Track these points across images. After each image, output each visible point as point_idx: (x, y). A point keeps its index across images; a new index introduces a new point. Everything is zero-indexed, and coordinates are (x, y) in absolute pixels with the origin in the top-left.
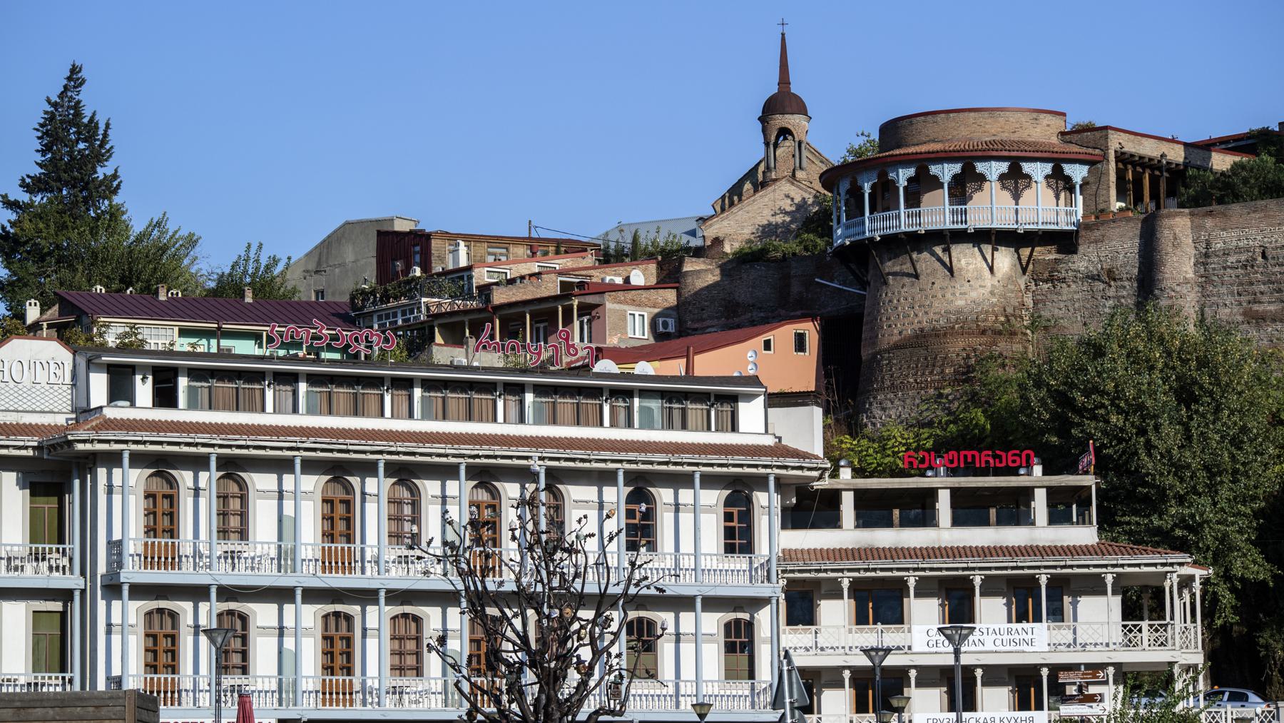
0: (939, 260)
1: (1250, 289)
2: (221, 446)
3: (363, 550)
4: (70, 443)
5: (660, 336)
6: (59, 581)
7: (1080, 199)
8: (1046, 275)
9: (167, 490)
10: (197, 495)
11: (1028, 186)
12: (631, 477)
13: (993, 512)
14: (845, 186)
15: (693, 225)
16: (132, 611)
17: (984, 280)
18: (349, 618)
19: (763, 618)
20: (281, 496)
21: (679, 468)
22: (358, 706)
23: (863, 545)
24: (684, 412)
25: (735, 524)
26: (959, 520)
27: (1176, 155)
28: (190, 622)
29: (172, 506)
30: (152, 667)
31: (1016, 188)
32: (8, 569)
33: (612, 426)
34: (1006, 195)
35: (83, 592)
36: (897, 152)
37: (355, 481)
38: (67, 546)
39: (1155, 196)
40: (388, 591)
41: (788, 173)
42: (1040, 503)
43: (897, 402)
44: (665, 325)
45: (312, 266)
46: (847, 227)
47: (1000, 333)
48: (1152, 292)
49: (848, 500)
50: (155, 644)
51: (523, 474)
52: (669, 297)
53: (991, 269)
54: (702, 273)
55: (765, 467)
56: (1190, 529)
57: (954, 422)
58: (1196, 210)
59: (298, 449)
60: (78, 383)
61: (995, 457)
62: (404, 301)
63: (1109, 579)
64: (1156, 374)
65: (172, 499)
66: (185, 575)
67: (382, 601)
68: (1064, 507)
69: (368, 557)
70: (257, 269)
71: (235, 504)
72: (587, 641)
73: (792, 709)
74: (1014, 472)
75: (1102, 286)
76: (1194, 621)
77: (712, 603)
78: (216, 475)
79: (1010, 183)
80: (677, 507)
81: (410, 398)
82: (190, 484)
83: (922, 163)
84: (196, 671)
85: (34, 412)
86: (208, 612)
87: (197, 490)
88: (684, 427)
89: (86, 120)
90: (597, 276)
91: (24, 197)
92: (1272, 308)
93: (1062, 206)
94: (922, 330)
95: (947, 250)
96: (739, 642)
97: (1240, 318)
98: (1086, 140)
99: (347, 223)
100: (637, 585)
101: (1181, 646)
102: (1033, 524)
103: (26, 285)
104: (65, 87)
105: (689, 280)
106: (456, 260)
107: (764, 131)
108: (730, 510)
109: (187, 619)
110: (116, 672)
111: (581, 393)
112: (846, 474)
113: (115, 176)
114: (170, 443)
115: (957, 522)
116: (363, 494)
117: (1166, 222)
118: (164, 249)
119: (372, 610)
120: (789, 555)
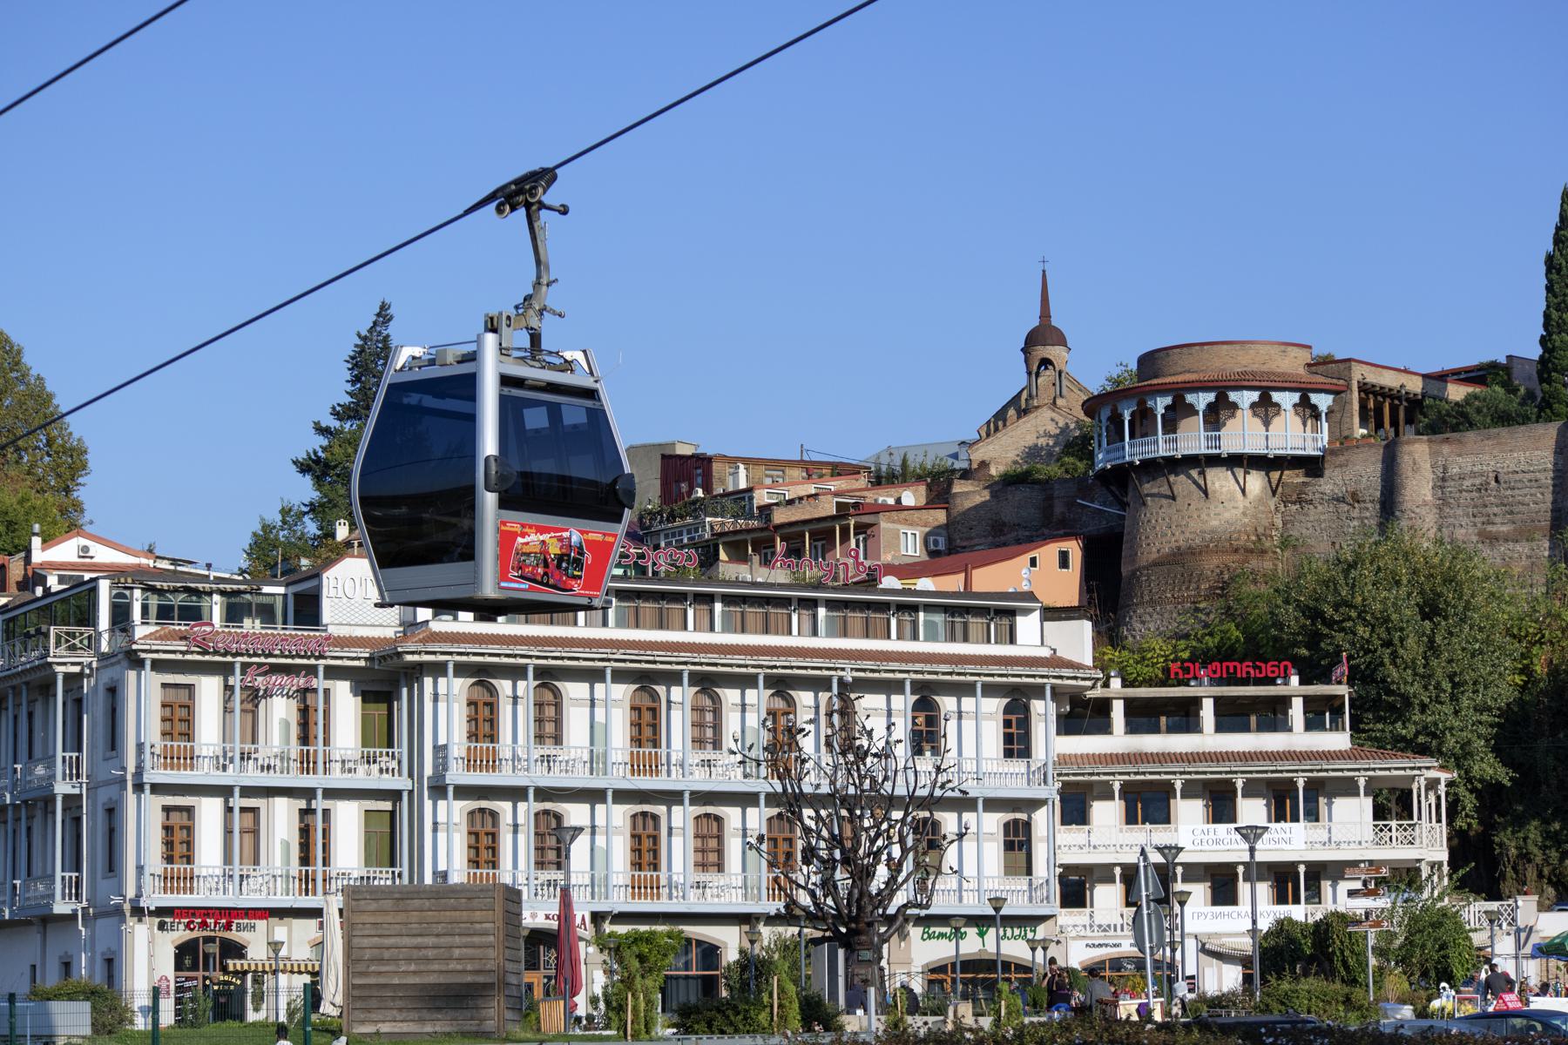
0: (1195, 482)
1: (1484, 511)
2: (538, 657)
3: (668, 755)
4: (399, 655)
5: (933, 554)
7: (1325, 425)
8: (1294, 497)
10: (516, 703)
11: (1278, 413)
12: (918, 687)
13: (1253, 719)
14: (1105, 413)
15: (955, 449)
16: (455, 811)
17: (1236, 501)
18: (655, 818)
19: (1040, 819)
20: (889, 714)
21: (962, 678)
22: (320, 896)
25: (1013, 730)
26: (1132, 728)
27: (1415, 386)
28: (510, 821)
29: (492, 712)
30: (474, 862)
31: (1267, 415)
32: (343, 771)
34: (1258, 422)
35: (411, 792)
36: (1155, 381)
37: (661, 690)
38: (396, 750)
39: (1395, 423)
40: (692, 793)
42: (1297, 711)
44: (936, 543)
46: (1108, 452)
47: (1252, 551)
48: (1393, 514)
50: (477, 841)
51: (818, 684)
52: (940, 516)
53: (1243, 491)
54: (970, 495)
56: (1434, 735)
57: (1211, 634)
58: (1433, 437)
59: (609, 660)
62: (689, 520)
63: (1362, 782)
64: (1403, 591)
65: (492, 706)
67: (687, 801)
68: (1320, 713)
69: (673, 761)
71: (550, 712)
72: (896, 839)
74: (1272, 682)
75: (1346, 508)
76: (1439, 821)
77: (993, 804)
78: (534, 684)
79: (1261, 411)
81: (712, 612)
82: (509, 692)
83: (1178, 393)
84: (515, 866)
86: (527, 810)
87: (515, 699)
88: (966, 639)
91: (334, 423)
92: (1504, 528)
94: (1179, 548)
95: (1202, 473)
96: (1018, 841)
97: (1475, 539)
98: (1329, 371)
100: (942, 787)
101: (1428, 844)
102: (1290, 730)
103: (335, 506)
104: (375, 323)
105: (958, 501)
106: (736, 482)
107: (1026, 361)
109: (506, 818)
110: (442, 867)
111: (865, 606)
114: (813, 668)
115: (1219, 728)
116: (669, 702)
117: (1406, 448)
119: (677, 810)
120: (1063, 760)
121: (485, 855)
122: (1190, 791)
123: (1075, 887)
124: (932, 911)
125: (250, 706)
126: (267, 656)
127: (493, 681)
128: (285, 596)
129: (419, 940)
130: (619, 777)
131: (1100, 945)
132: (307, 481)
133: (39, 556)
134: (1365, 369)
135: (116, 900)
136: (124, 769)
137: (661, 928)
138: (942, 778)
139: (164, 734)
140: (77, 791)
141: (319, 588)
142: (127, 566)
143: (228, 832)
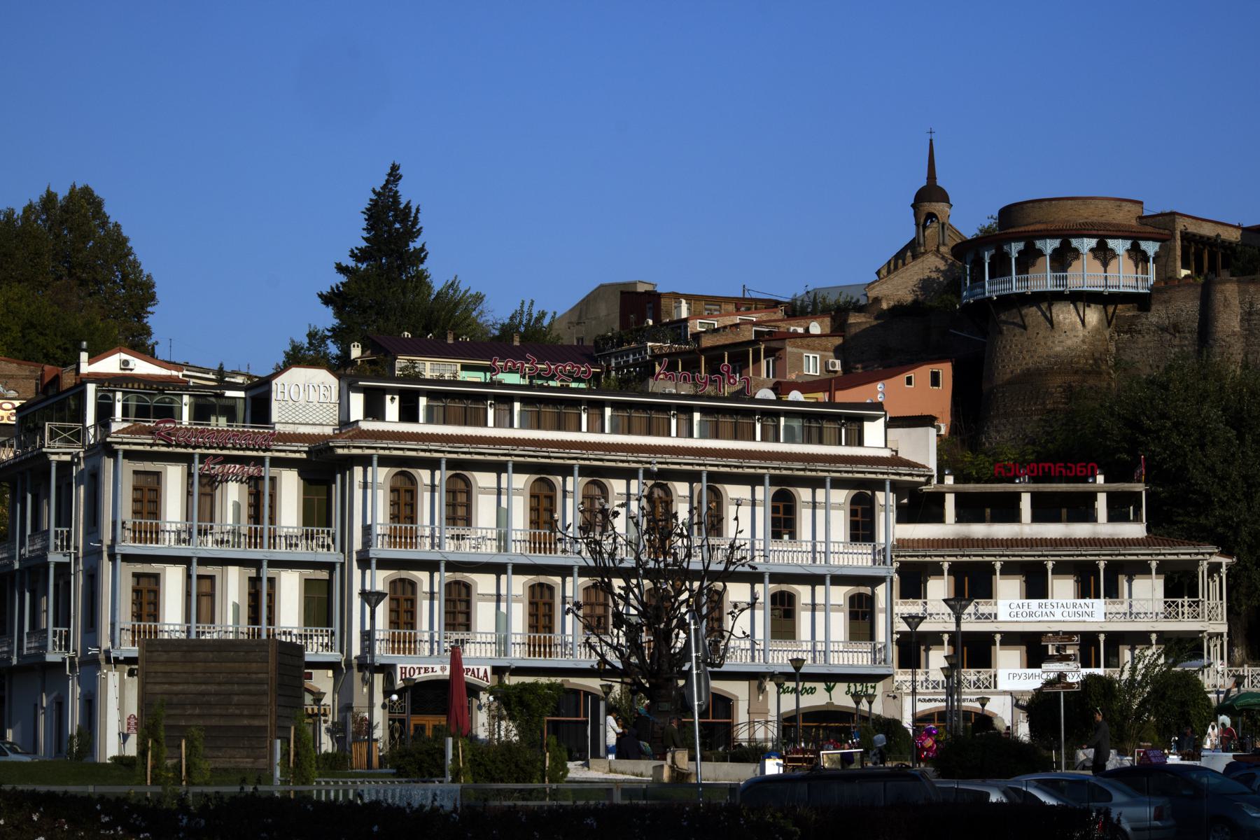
2: (450, 452)
6: (322, 555)
9: (409, 487)
13: (1064, 511)
14: (970, 257)
17: (1078, 328)
18: (551, 588)
23: (961, 536)
24: (820, 429)
25: (781, 515)
27: (1234, 236)
31: (1105, 258)
33: (588, 431)
41: (934, 249)
42: (1101, 503)
45: (574, 319)
49: (950, 501)
51: (692, 477)
52: (838, 341)
55: (883, 473)
60: (344, 406)
61: (1067, 468)
66: (424, 551)
70: (530, 320)
71: (462, 498)
73: (697, 663)
76: (1221, 599)
77: (839, 580)
79: (1101, 254)
80: (814, 505)
85: (307, 424)
87: (433, 488)
89: (402, 206)
90: (783, 327)
91: (351, 263)
93: (1140, 275)
96: (861, 615)
98: (1160, 226)
99: (602, 286)
104: (387, 181)
107: (915, 215)
108: (855, 507)
111: (737, 417)
112: (949, 480)
113: (422, 249)
117: (1219, 287)
118: (457, 304)
120: (902, 544)
121: (404, 617)
122: (1009, 569)
123: (911, 649)
124: (724, 669)
125: (208, 489)
126: (222, 449)
127: (791, 489)
128: (245, 399)
129: (203, 687)
130: (518, 552)
131: (930, 700)
132: (329, 311)
133: (85, 368)
134: (1187, 221)
135: (94, 651)
136: (101, 542)
137: (544, 680)
138: (738, 555)
139: (135, 513)
140: (66, 560)
141: (269, 392)
142: (160, 377)
143: (188, 594)
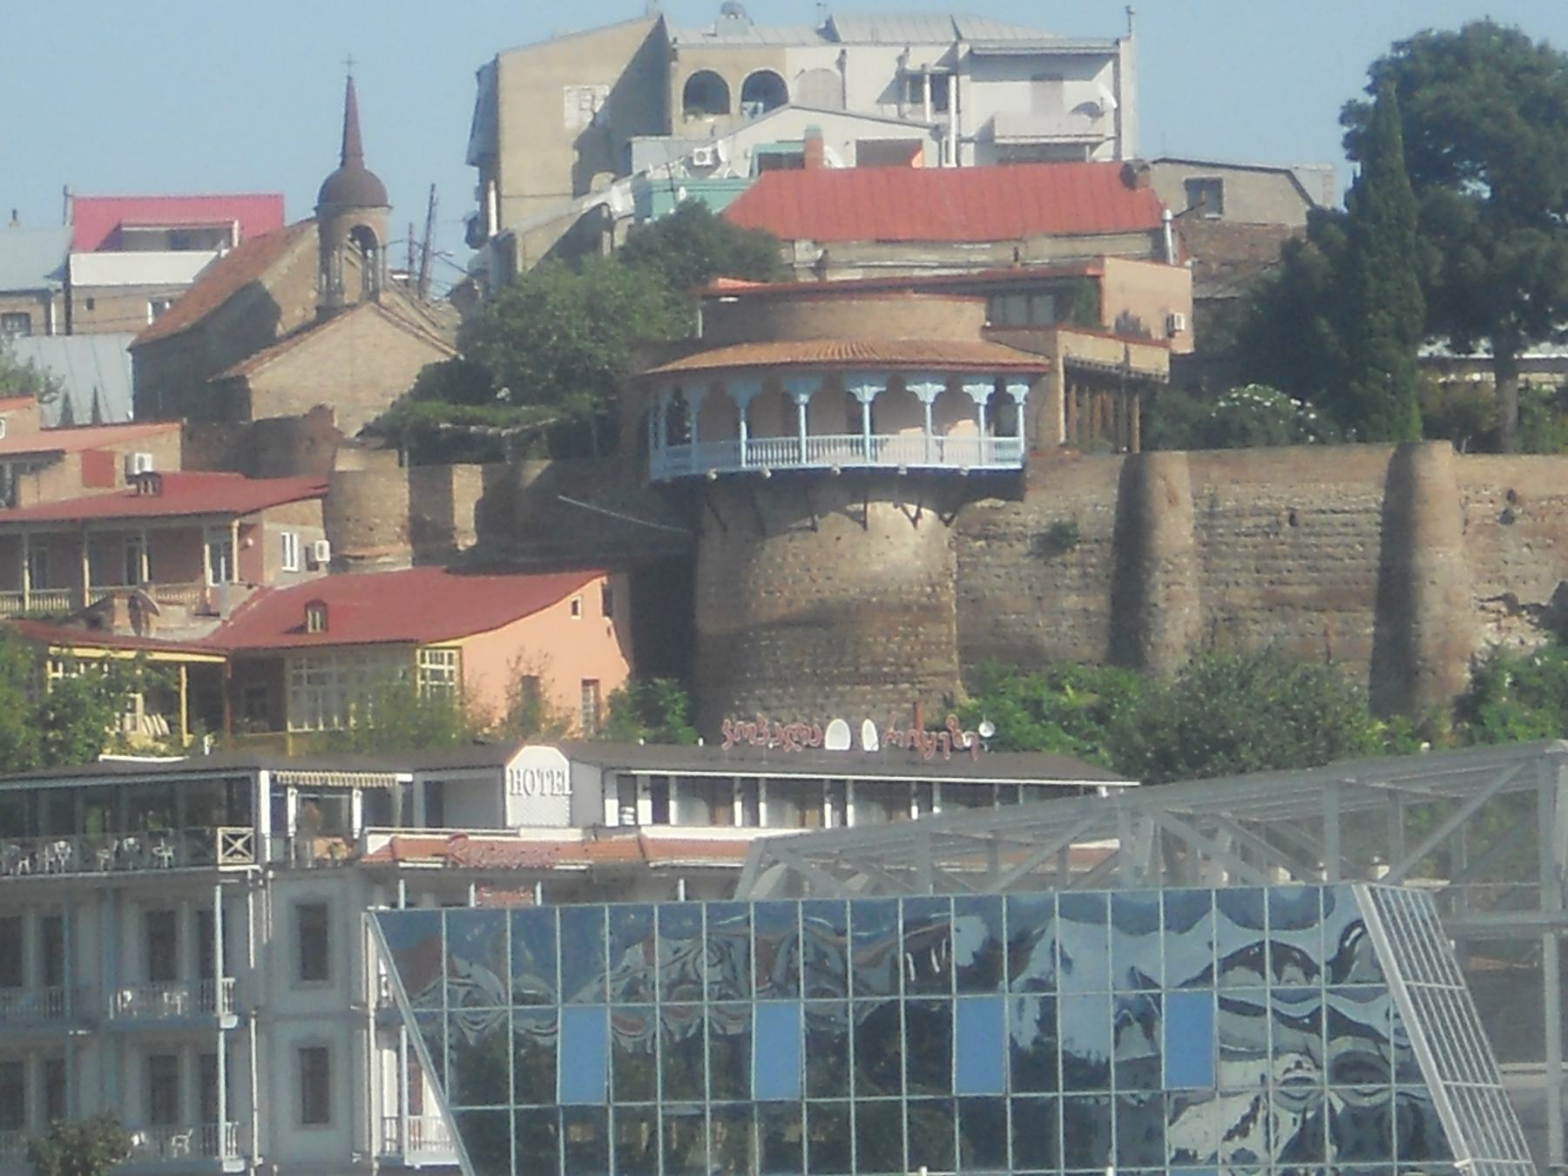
43: (788, 701)
92: (1304, 591)
